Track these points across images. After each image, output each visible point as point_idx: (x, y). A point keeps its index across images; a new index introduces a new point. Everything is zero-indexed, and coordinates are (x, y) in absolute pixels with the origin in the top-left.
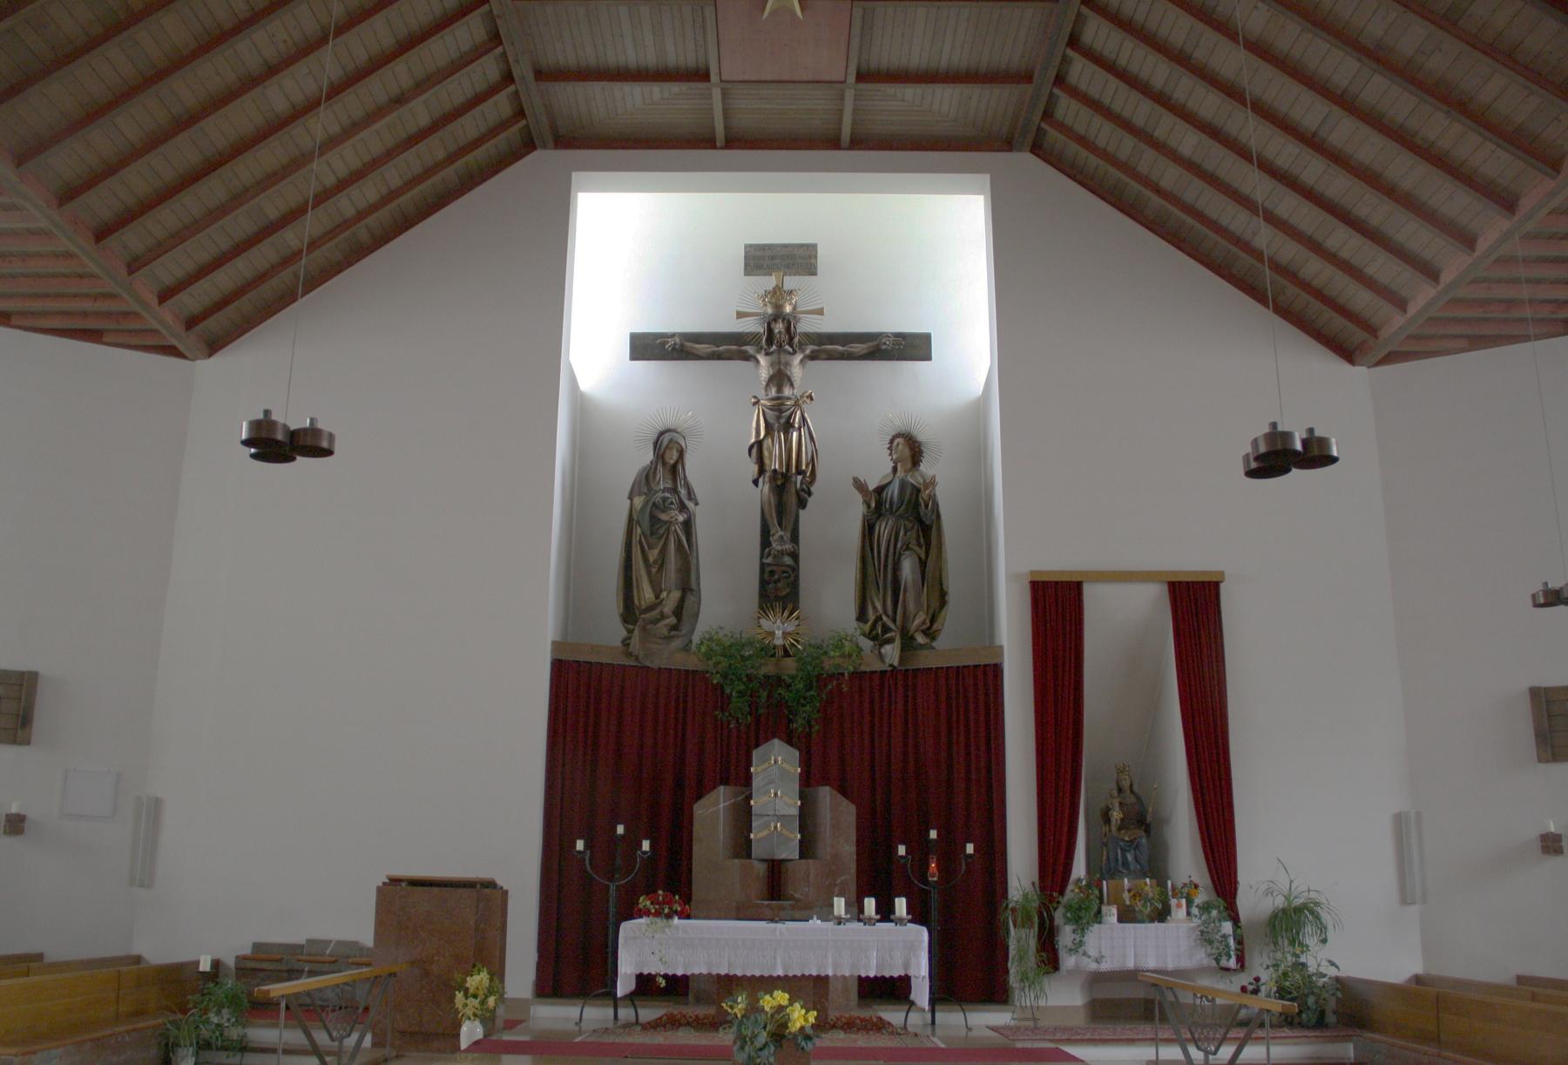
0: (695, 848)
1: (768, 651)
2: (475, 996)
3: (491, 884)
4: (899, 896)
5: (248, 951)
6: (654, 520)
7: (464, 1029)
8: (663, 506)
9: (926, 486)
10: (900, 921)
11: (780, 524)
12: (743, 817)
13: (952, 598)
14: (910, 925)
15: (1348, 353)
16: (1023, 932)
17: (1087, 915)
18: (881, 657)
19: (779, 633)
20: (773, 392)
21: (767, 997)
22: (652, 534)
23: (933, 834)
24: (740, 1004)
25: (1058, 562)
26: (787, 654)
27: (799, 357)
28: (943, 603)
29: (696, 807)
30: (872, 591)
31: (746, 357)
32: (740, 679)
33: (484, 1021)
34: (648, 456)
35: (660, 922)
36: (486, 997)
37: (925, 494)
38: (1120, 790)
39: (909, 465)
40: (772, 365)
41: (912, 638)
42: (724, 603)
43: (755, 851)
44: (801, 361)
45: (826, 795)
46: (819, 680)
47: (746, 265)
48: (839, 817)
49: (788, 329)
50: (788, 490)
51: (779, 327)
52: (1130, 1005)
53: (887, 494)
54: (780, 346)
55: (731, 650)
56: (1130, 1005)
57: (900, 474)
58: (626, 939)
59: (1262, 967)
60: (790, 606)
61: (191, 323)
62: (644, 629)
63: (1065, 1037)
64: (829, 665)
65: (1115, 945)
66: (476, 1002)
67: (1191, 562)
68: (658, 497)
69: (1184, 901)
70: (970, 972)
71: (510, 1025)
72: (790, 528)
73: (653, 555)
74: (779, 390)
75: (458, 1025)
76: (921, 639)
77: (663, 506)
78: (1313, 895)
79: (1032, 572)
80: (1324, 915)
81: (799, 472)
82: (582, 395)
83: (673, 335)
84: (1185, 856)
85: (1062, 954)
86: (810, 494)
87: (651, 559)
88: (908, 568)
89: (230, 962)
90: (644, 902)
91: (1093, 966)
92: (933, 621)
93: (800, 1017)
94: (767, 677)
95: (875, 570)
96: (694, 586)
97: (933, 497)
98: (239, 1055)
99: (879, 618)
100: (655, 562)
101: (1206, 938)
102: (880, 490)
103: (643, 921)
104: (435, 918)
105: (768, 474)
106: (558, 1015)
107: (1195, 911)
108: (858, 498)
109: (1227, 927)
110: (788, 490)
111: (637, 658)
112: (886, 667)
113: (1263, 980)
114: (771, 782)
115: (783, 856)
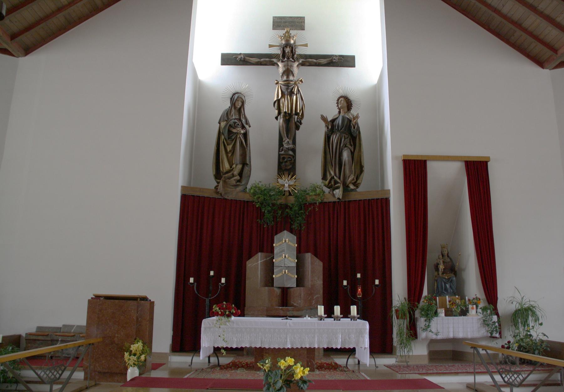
0: (247, 282)
1: (282, 193)
2: (135, 355)
3: (145, 299)
4: (337, 305)
5: (33, 330)
6: (230, 132)
7: (129, 371)
8: (234, 126)
9: (354, 118)
10: (353, 318)
11: (288, 137)
12: (270, 267)
13: (366, 169)
14: (358, 320)
15: (541, 63)
16: (401, 321)
17: (431, 313)
18: (334, 195)
19: (286, 185)
20: (285, 78)
21: (282, 361)
22: (229, 139)
23: (359, 276)
24: (267, 364)
25: (416, 150)
26: (290, 194)
27: (296, 64)
28: (362, 171)
29: (247, 262)
30: (329, 166)
31: (273, 64)
32: (269, 205)
33: (139, 368)
34: (228, 105)
35: (224, 319)
36: (141, 355)
37: (353, 122)
38: (443, 256)
39: (346, 110)
40: (284, 66)
41: (348, 186)
42: (262, 171)
43: (275, 284)
44: (298, 66)
45: (308, 257)
46: (305, 206)
47: (273, 25)
48: (314, 267)
49: (292, 51)
50: (291, 121)
51: (288, 50)
52: (450, 355)
53: (336, 122)
54: (288, 58)
55: (263, 192)
56: (450, 355)
57: (342, 114)
58: (205, 328)
59: (508, 336)
60: (292, 174)
61: (13, 37)
62: (225, 182)
63: (424, 372)
64: (309, 199)
65: (445, 327)
66: (135, 358)
67: (475, 152)
68: (231, 122)
69: (475, 306)
70: (381, 344)
71: (156, 367)
72: (292, 138)
73: (229, 148)
74: (288, 77)
75: (126, 369)
76: (352, 187)
77: (234, 126)
78: (532, 303)
79: (404, 155)
80: (538, 313)
81: (297, 114)
82: (199, 80)
83: (240, 54)
84: (473, 286)
85: (419, 330)
86: (301, 124)
87: (228, 150)
88: (346, 155)
89: (24, 335)
90: (216, 308)
91: (434, 337)
92: (357, 179)
93: (300, 372)
94: (281, 204)
95: (331, 157)
96: (248, 162)
97: (357, 123)
98: (16, 385)
99: (333, 178)
100: (230, 151)
101: (485, 323)
102: (333, 121)
103: (215, 318)
104: (118, 315)
105: (282, 114)
106: (181, 360)
107: (480, 310)
108: (323, 124)
109: (495, 318)
110: (291, 121)
111: (221, 195)
112: (335, 200)
113: (512, 342)
114: (283, 251)
115: (288, 286)
